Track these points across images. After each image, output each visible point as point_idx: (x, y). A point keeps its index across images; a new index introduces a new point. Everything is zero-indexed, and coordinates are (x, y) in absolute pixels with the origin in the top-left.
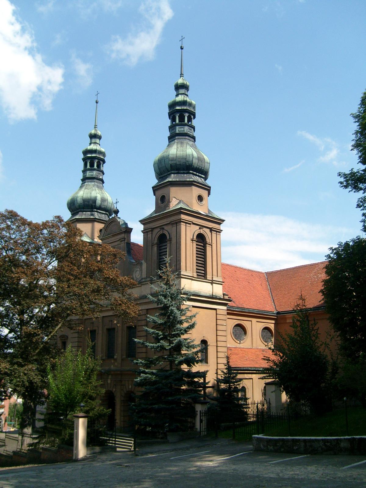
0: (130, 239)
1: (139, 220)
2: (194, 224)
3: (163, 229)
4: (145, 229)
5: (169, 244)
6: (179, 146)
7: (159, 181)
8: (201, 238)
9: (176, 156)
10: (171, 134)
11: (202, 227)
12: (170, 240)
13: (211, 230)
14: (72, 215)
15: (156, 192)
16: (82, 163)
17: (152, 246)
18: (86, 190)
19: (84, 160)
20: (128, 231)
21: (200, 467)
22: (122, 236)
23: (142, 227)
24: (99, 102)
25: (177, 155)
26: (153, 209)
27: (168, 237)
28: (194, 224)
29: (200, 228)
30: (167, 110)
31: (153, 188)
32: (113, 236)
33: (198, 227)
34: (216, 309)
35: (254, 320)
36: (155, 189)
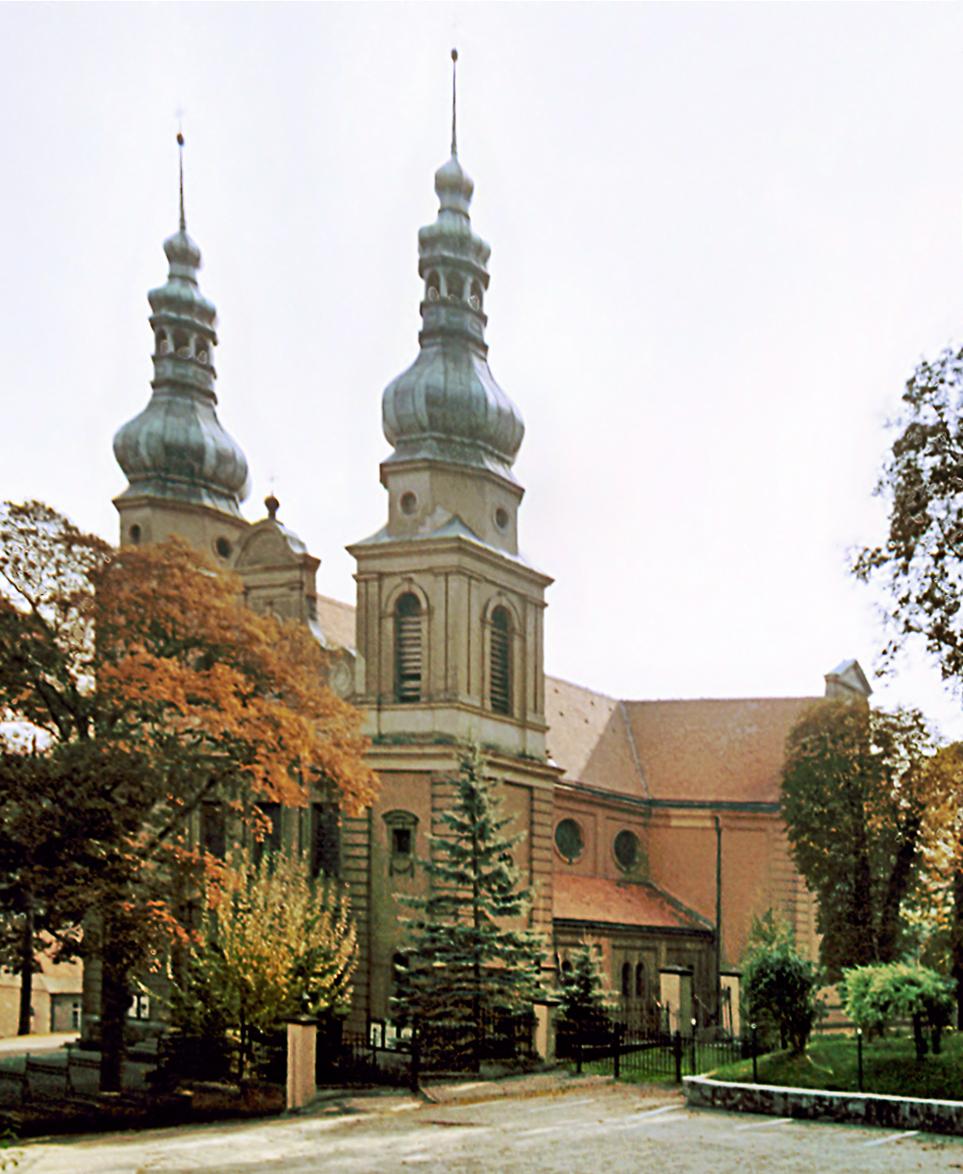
0: (314, 587)
1: (351, 542)
2: (487, 581)
3: (410, 580)
4: (360, 572)
5: (376, 584)
6: (451, 365)
7: (398, 452)
8: (501, 618)
9: (445, 395)
10: (426, 323)
11: (503, 590)
12: (430, 611)
13: (523, 598)
14: (131, 481)
15: (391, 480)
16: (151, 335)
17: (380, 619)
18: (171, 419)
19: (153, 323)
20: (310, 565)
21: (452, 1093)
22: (295, 574)
23: (351, 565)
24: (922, 709)
25: (449, 394)
26: (382, 518)
27: (424, 605)
28: (487, 581)
29: (499, 594)
30: (414, 257)
31: (382, 466)
32: (268, 569)
33: (495, 590)
34: (530, 788)
35: (600, 813)
36: (386, 472)
